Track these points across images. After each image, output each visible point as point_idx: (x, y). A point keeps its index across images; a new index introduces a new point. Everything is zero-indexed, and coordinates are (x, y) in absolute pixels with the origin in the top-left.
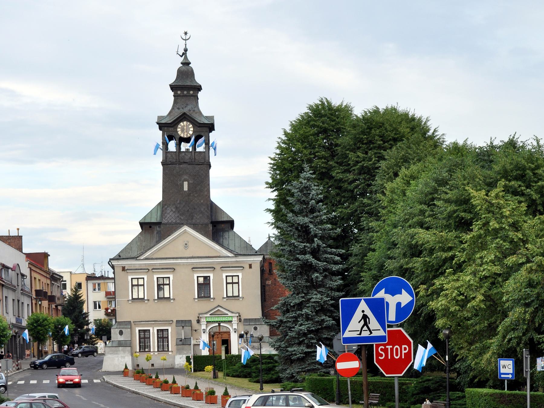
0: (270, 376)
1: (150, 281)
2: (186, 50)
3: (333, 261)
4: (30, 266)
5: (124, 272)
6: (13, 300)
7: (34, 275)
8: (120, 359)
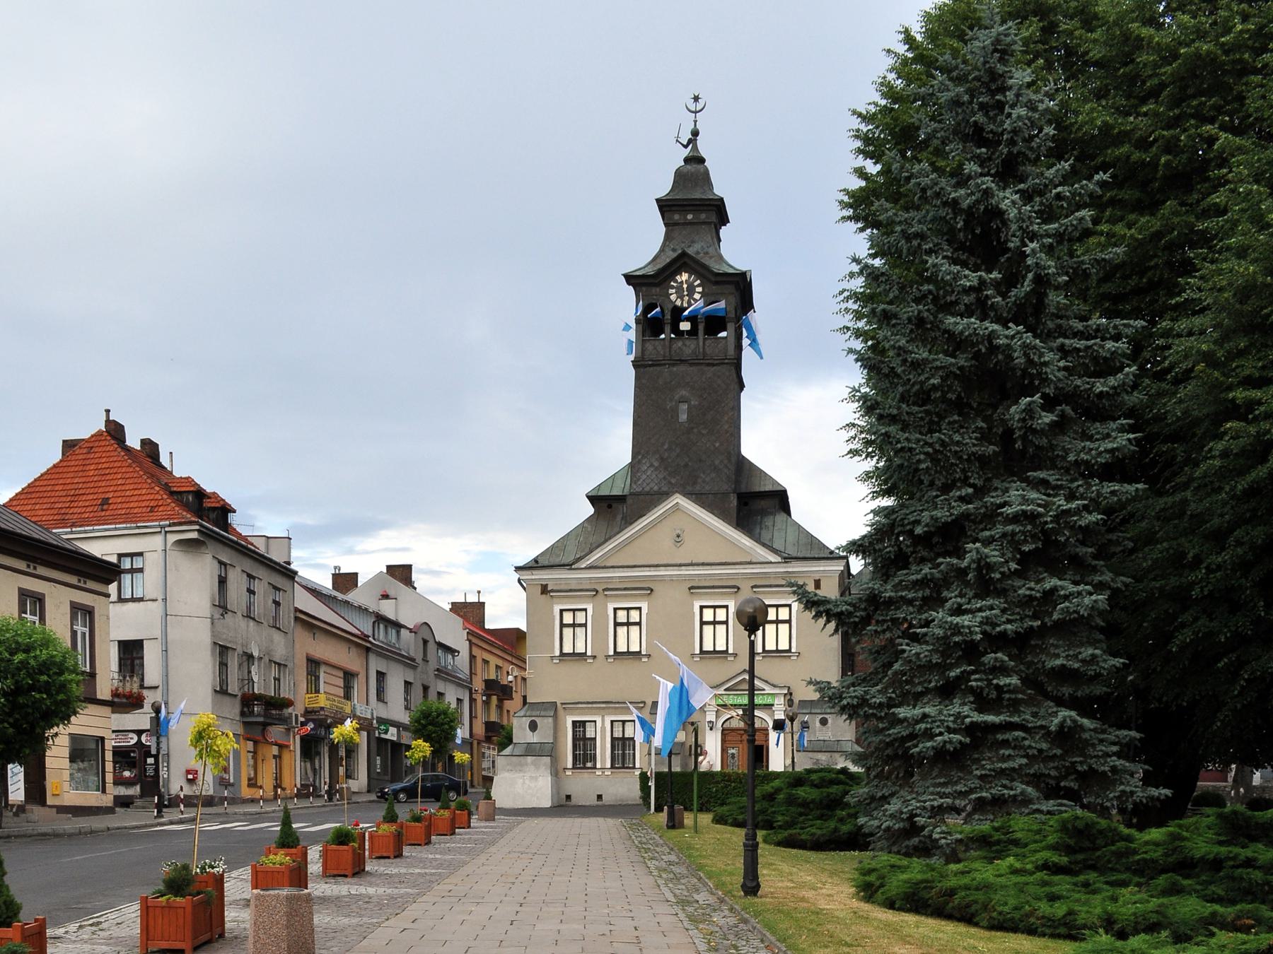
0: (832, 824)
1: (600, 616)
2: (695, 133)
3: (1095, 359)
4: (470, 637)
6: (407, 684)
7: (476, 651)
8: (527, 782)
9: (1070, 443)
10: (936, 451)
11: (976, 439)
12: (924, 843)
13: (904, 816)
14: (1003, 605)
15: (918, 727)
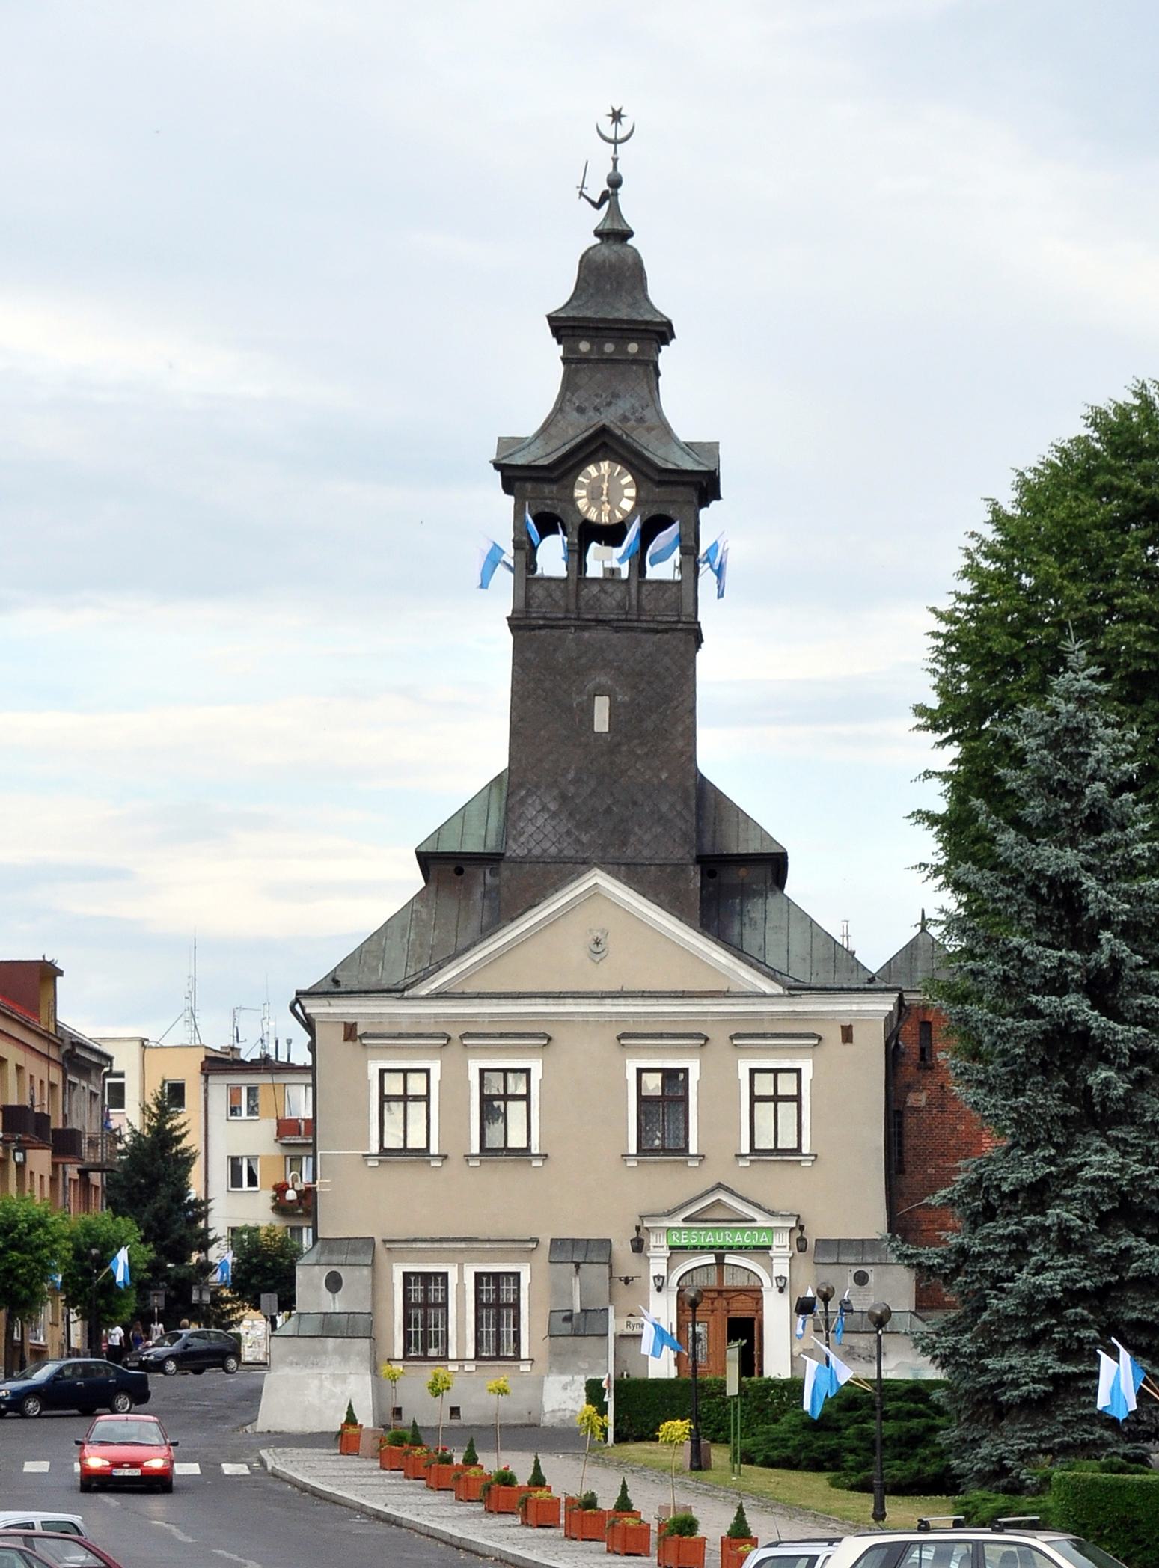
0: (915, 1465)
1: (454, 1083)
2: (615, 182)
5: (350, 1043)
8: (327, 1384)
9: (1148, 1101)
10: (1020, 1115)
11: (1059, 1099)
12: (1013, 1484)
13: (994, 1459)
14: (1082, 1263)
15: (1005, 1377)
